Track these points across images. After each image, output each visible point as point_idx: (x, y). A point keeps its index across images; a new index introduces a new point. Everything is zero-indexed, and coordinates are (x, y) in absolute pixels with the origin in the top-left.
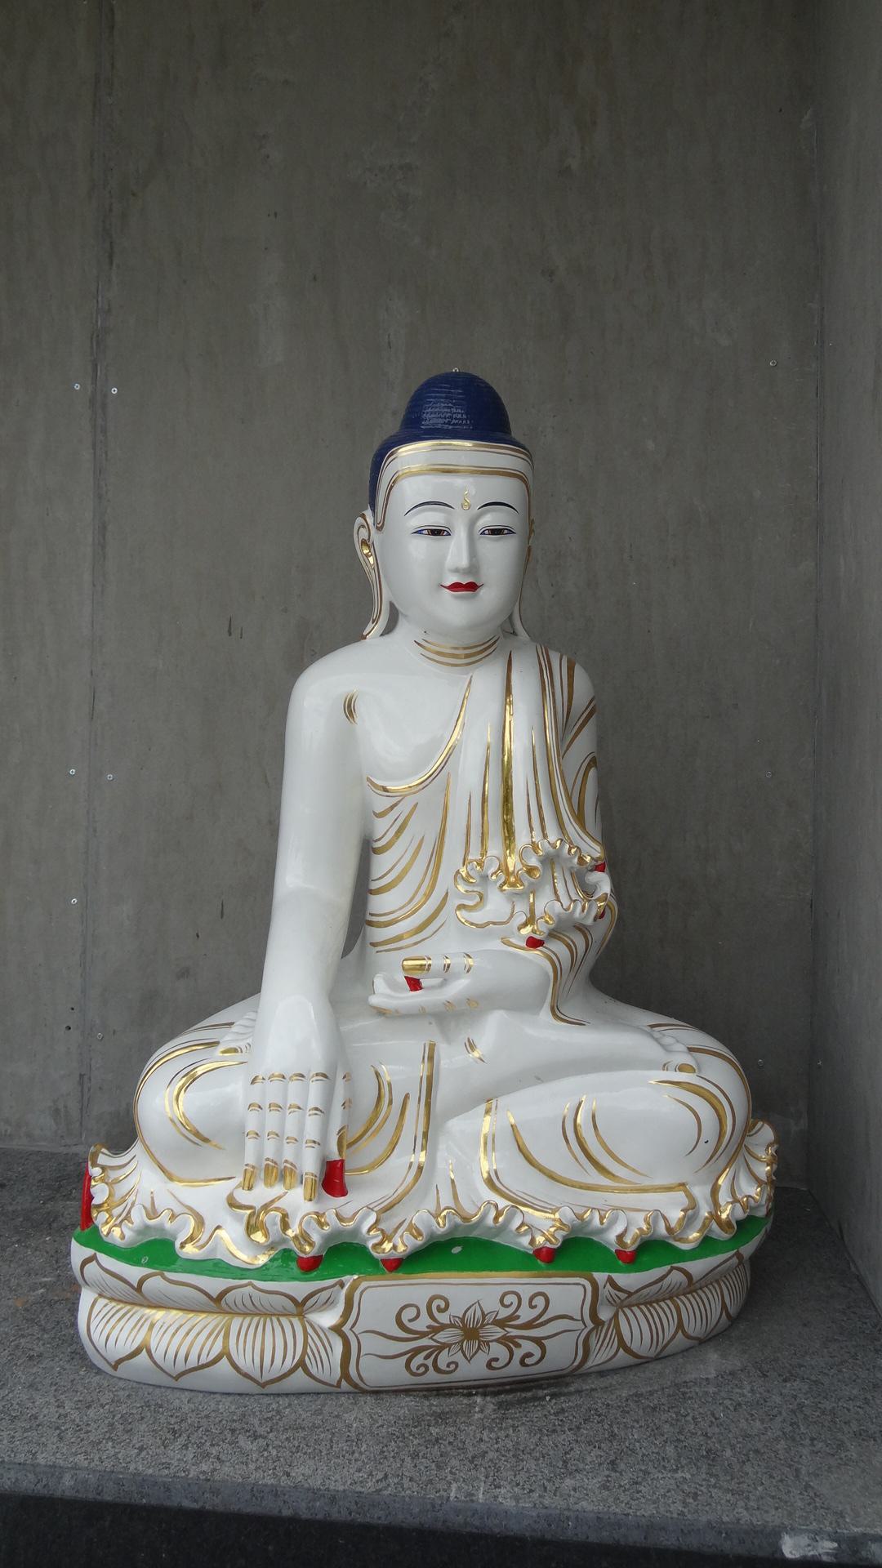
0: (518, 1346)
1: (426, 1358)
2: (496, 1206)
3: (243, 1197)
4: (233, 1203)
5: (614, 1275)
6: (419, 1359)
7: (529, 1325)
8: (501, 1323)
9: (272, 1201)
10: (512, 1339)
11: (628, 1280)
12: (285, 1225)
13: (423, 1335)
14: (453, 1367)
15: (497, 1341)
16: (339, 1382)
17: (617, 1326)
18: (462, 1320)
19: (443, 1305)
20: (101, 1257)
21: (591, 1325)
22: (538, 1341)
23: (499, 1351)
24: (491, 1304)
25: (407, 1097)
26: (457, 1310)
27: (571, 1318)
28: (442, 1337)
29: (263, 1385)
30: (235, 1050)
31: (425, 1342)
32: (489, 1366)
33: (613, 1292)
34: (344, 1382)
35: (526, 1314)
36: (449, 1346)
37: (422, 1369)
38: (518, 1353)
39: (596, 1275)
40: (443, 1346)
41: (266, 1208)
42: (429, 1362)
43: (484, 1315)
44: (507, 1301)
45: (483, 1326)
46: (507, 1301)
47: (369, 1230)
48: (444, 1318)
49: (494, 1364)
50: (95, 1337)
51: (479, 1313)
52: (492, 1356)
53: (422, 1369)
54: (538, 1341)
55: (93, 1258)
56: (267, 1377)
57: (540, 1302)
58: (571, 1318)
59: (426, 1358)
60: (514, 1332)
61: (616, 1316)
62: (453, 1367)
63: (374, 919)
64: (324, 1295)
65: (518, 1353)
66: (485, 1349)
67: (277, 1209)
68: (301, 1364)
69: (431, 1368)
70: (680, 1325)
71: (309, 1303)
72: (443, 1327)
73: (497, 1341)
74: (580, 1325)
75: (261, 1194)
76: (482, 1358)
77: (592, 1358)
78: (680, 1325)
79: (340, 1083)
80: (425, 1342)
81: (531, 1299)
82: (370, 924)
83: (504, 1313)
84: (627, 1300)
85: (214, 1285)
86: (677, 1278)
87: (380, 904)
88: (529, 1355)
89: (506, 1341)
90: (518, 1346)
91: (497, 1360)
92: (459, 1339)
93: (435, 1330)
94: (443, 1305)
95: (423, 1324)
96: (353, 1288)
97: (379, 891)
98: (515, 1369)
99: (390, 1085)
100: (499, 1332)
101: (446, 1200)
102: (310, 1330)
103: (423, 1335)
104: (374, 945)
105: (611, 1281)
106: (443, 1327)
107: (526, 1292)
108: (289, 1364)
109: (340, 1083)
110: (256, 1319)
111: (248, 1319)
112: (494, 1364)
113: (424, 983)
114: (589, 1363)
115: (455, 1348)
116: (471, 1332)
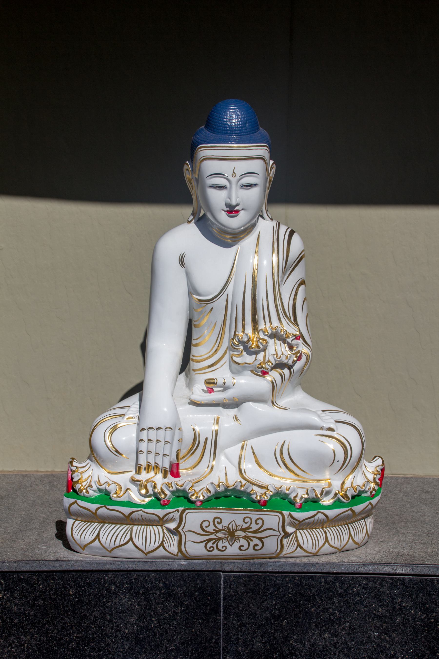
0: (252, 540)
1: (213, 543)
2: (241, 483)
3: (138, 477)
4: (133, 481)
5: (292, 513)
6: (210, 544)
7: (256, 532)
8: (244, 530)
9: (150, 479)
10: (249, 537)
11: (300, 515)
12: (155, 487)
13: (211, 533)
14: (224, 548)
15: (242, 537)
16: (178, 553)
17: (296, 537)
18: (228, 528)
19: (219, 521)
20: (79, 502)
21: (283, 534)
22: (260, 539)
23: (243, 542)
24: (239, 521)
25: (207, 438)
26: (225, 523)
27: (274, 530)
28: (219, 535)
29: (146, 554)
30: (132, 418)
31: (213, 536)
32: (240, 549)
33: (292, 520)
34: (179, 554)
35: (254, 527)
36: (223, 539)
37: (212, 549)
38: (252, 544)
39: (284, 512)
40: (220, 539)
41: (147, 481)
42: (214, 546)
43: (237, 526)
44: (246, 520)
45: (236, 531)
46: (246, 520)
47: (189, 489)
48: (220, 527)
49: (242, 548)
50: (75, 536)
51: (234, 525)
52: (241, 544)
53: (212, 549)
54: (260, 539)
55: (76, 502)
56: (148, 550)
57: (260, 522)
58: (274, 530)
59: (213, 543)
60: (250, 534)
61: (295, 532)
62: (224, 548)
63: (194, 358)
64: (171, 515)
65: (252, 544)
66: (238, 541)
67: (153, 481)
68: (162, 544)
69: (215, 548)
70: (327, 540)
71: (165, 519)
72: (220, 530)
73: (242, 537)
74: (278, 534)
75: (144, 476)
76: (236, 545)
77: (285, 549)
78: (327, 540)
79: (177, 431)
80: (213, 536)
81: (256, 520)
82: (193, 360)
83: (245, 526)
84: (300, 525)
85: (127, 510)
86: (320, 516)
87: (195, 351)
88: (257, 545)
89: (246, 538)
90: (252, 540)
91: (243, 546)
92: (227, 536)
93: (217, 531)
94: (219, 521)
95: (211, 528)
96: (183, 511)
97: (196, 345)
98: (251, 551)
99: (245, 456)
100: (243, 534)
101: (223, 480)
102: (165, 531)
103: (211, 533)
104: (194, 370)
105: (290, 514)
106: (220, 530)
107: (254, 517)
108: (157, 544)
109: (177, 431)
110: (143, 526)
111: (140, 526)
112: (242, 548)
113: (215, 389)
114: (284, 553)
115: (225, 540)
116: (232, 533)
